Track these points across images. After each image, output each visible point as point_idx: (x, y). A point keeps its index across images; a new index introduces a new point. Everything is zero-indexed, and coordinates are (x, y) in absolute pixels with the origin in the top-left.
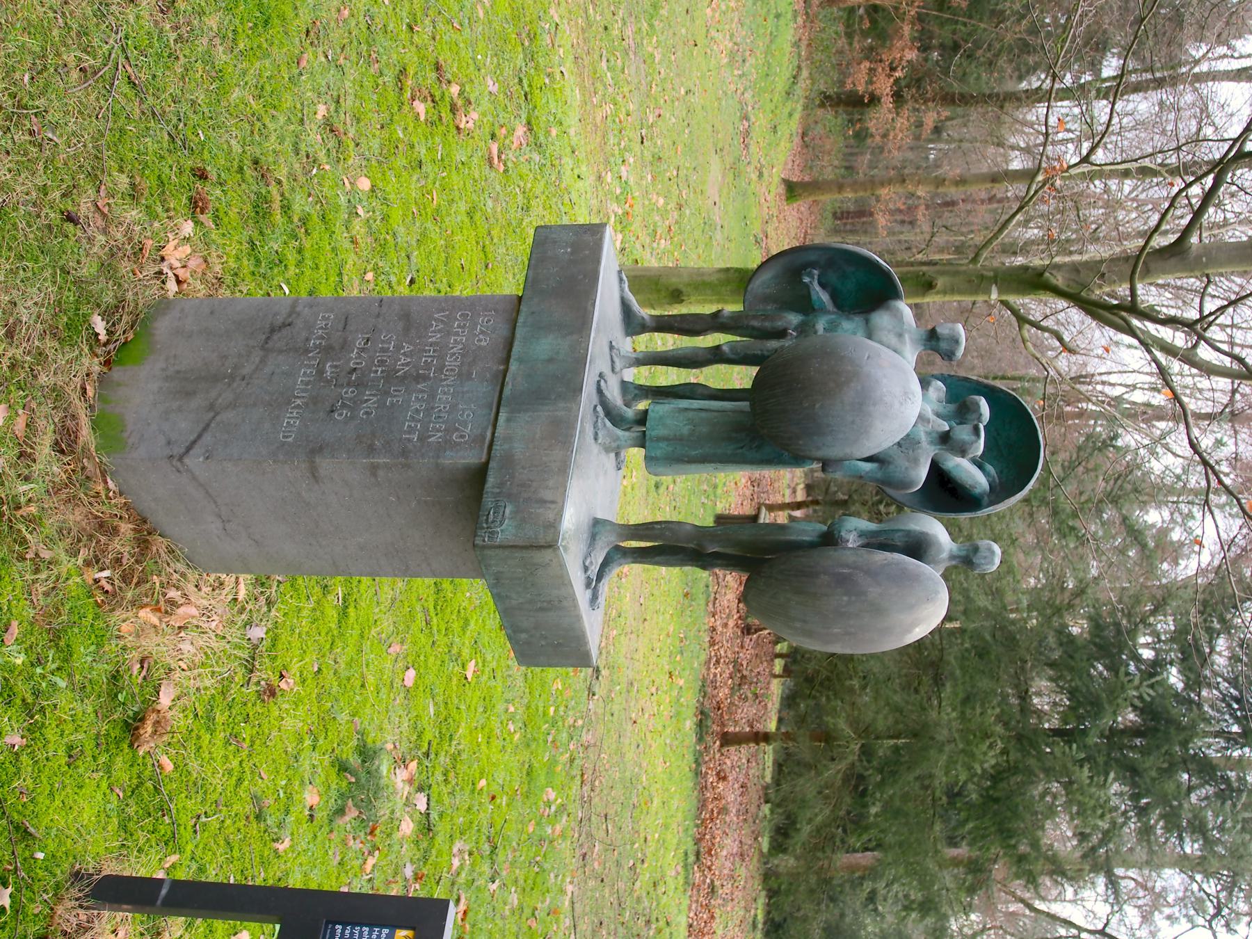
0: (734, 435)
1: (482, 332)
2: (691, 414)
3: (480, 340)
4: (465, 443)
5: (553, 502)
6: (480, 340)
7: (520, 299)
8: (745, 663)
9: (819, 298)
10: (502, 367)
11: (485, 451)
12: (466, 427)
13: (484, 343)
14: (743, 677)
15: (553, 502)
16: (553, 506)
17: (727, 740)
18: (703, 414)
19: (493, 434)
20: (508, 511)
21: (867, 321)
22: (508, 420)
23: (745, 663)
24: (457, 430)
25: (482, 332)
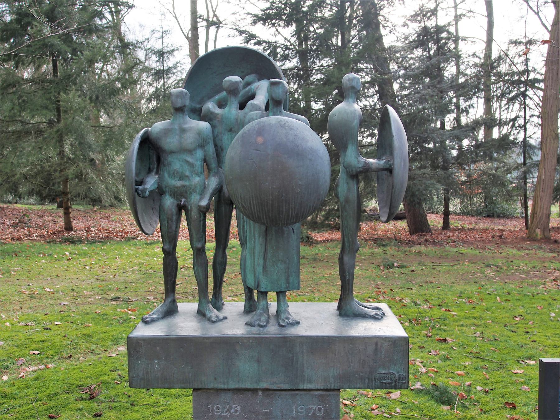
0: (285, 235)
1: (228, 411)
2: (268, 263)
3: (236, 411)
4: (324, 407)
5: (376, 344)
6: (236, 411)
7: (194, 390)
8: (12, 222)
9: (153, 184)
10: (260, 393)
11: (330, 393)
12: (312, 408)
13: (239, 408)
14: (20, 222)
15: (376, 344)
16: (379, 344)
17: (69, 227)
18: (269, 255)
19: (318, 390)
20: (384, 372)
21: (172, 152)
22: (310, 382)
23: (12, 222)
24: (314, 414)
25: (228, 411)
